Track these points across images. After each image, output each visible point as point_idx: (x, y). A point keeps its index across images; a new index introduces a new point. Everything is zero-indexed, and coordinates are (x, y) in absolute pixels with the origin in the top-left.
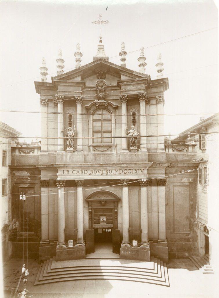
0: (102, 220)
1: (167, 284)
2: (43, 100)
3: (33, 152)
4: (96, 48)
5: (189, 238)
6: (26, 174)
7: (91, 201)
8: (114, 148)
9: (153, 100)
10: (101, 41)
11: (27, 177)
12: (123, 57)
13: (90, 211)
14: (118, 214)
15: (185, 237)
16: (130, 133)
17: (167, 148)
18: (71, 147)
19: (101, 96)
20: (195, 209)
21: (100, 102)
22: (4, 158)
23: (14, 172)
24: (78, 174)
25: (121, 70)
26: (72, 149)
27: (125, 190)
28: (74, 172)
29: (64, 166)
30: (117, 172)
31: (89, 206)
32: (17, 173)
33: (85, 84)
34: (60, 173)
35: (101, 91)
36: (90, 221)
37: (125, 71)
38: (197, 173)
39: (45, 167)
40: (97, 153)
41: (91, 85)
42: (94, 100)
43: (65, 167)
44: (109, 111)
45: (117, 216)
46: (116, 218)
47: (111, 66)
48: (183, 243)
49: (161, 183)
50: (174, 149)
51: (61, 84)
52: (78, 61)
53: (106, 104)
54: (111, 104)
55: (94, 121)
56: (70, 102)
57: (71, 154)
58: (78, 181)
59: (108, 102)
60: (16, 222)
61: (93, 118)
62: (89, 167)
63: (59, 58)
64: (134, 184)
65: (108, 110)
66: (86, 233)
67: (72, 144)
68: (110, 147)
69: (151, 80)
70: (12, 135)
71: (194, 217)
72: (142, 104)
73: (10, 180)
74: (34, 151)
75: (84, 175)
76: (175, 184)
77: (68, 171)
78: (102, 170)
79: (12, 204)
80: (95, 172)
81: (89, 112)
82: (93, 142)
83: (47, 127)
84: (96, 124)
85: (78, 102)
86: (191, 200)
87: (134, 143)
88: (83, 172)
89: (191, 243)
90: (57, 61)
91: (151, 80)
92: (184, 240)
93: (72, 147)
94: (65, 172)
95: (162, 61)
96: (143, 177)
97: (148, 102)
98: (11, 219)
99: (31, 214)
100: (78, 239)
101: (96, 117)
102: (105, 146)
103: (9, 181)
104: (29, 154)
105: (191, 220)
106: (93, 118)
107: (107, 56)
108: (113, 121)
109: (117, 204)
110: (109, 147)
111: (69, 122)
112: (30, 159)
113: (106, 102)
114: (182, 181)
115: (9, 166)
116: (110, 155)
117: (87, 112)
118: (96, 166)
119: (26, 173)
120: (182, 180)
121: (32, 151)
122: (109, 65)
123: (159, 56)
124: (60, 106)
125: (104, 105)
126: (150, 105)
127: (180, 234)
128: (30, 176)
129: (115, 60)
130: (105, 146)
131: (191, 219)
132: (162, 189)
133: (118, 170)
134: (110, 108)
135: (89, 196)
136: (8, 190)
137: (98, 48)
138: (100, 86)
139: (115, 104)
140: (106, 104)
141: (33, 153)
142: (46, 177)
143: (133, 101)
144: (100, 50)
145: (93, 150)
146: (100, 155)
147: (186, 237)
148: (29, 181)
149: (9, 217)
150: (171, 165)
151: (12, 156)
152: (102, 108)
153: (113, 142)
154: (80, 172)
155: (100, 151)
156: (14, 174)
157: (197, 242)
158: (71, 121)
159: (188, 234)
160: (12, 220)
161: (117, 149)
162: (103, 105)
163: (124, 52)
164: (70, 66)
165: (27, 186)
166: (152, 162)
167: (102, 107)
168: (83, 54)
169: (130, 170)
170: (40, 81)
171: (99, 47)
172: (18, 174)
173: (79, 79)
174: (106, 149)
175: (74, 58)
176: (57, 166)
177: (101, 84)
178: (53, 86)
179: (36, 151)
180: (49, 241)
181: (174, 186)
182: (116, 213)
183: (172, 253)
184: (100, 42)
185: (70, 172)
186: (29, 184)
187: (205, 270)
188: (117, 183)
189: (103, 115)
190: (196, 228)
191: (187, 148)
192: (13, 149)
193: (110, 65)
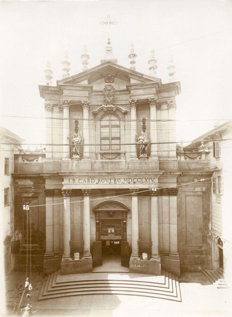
1: (178, 299)
3: (37, 159)
5: (202, 251)
6: (29, 183)
7: (99, 212)
8: (122, 155)
9: (165, 105)
10: (109, 43)
11: (30, 186)
12: (132, 59)
13: (98, 222)
15: (198, 250)
16: (139, 140)
17: (179, 155)
18: (77, 154)
19: (109, 101)
22: (6, 166)
23: (17, 181)
24: (85, 183)
25: (130, 73)
26: (78, 157)
27: (135, 199)
28: (80, 181)
29: (70, 174)
32: (20, 182)
34: (66, 181)
36: (98, 233)
38: (210, 182)
40: (104, 160)
42: (102, 105)
43: (71, 175)
45: (126, 227)
47: (120, 69)
49: (172, 192)
50: (186, 157)
51: (67, 88)
52: (85, 63)
53: (114, 109)
55: (102, 127)
57: (77, 161)
58: (85, 190)
60: (19, 234)
64: (144, 194)
65: (117, 116)
67: (78, 151)
68: (119, 154)
73: (13, 189)
74: (38, 158)
76: (187, 193)
77: (74, 180)
80: (103, 181)
82: (101, 150)
84: (103, 130)
88: (90, 180)
89: (204, 256)
93: (78, 155)
94: (71, 181)
98: (14, 230)
99: (35, 225)
100: (84, 251)
101: (104, 123)
103: (11, 191)
104: (33, 162)
105: (204, 232)
111: (76, 128)
112: (34, 167)
113: (114, 108)
114: (195, 191)
116: (118, 163)
118: (104, 174)
119: (30, 181)
124: (66, 111)
125: (112, 110)
126: (161, 110)
129: (124, 63)
130: (114, 154)
134: (118, 113)
136: (10, 200)
137: (106, 50)
139: (124, 109)
141: (37, 160)
143: (143, 106)
146: (108, 162)
147: (200, 250)
148: (33, 190)
149: (11, 228)
150: (183, 174)
151: (15, 164)
154: (87, 180)
155: (108, 158)
156: (17, 183)
157: (210, 255)
159: (201, 246)
160: (15, 232)
162: (111, 110)
164: (76, 69)
166: (163, 170)
169: (140, 179)
172: (21, 183)
173: (85, 83)
174: (114, 157)
176: (63, 174)
177: (109, 88)
179: (40, 158)
180: (53, 254)
181: (186, 196)
185: (77, 181)
186: (33, 194)
187: (219, 284)
190: (210, 240)
191: (200, 155)
192: (16, 157)
193: (119, 68)
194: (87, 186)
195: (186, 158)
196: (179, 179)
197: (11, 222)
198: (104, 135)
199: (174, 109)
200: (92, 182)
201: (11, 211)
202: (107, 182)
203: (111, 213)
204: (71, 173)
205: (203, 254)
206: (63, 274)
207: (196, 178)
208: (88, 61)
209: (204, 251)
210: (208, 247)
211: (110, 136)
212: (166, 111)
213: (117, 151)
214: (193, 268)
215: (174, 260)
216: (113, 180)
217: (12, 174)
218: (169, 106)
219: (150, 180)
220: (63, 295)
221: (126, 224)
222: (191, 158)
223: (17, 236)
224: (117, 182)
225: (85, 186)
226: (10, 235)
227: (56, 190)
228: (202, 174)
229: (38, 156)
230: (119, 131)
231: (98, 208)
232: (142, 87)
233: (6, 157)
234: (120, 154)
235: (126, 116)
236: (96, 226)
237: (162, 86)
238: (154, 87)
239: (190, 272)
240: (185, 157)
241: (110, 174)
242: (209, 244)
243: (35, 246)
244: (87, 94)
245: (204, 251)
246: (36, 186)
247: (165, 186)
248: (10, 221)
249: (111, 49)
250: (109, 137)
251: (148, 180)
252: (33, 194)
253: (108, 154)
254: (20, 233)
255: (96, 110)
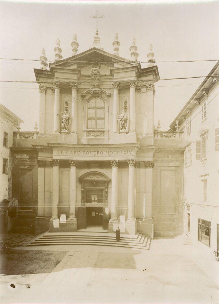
0: (94, 200)
3: (32, 136)
6: (26, 156)
7: (85, 182)
8: (106, 133)
10: (97, 34)
11: (26, 160)
13: (83, 190)
14: (109, 193)
18: (66, 129)
21: (95, 90)
22: (5, 140)
23: (14, 155)
25: (113, 59)
26: (66, 131)
27: (115, 169)
28: (68, 153)
29: (58, 145)
30: (108, 154)
31: (81, 186)
32: (17, 156)
33: (79, 71)
34: (55, 152)
36: (83, 200)
37: (117, 59)
40: (91, 137)
41: (87, 74)
43: (59, 146)
44: (102, 99)
45: (108, 195)
46: (106, 198)
47: (104, 55)
49: (150, 165)
51: (58, 71)
53: (100, 92)
54: (105, 92)
56: (65, 89)
57: (65, 135)
58: (71, 161)
60: (16, 201)
61: (123, 233)
62: (82, 148)
63: (56, 47)
64: (122, 165)
67: (67, 127)
68: (103, 132)
69: (142, 68)
72: (132, 90)
73: (11, 162)
74: (33, 135)
76: (163, 168)
77: (62, 152)
78: (94, 152)
79: (13, 184)
80: (88, 153)
81: (84, 100)
82: (87, 128)
85: (73, 88)
87: (123, 125)
88: (77, 152)
89: (176, 223)
90: (55, 51)
91: (142, 68)
94: (60, 152)
97: (138, 89)
98: (11, 197)
99: (29, 193)
103: (10, 162)
104: (29, 139)
106: (123, 233)
108: (106, 109)
109: (108, 184)
110: (102, 132)
111: (65, 107)
112: (28, 144)
113: (100, 91)
114: (169, 166)
115: (10, 148)
116: (102, 139)
117: (83, 99)
118: (88, 147)
119: (26, 155)
122: (103, 54)
128: (29, 159)
129: (108, 49)
132: (149, 170)
133: (108, 152)
136: (8, 170)
137: (94, 40)
138: (94, 75)
141: (32, 137)
144: (96, 42)
146: (93, 139)
148: (28, 163)
151: (14, 140)
152: (96, 96)
153: (105, 128)
154: (73, 152)
156: (15, 157)
157: (181, 222)
158: (67, 108)
159: (173, 214)
160: (12, 198)
163: (117, 42)
164: (67, 54)
166: (141, 148)
167: (96, 95)
169: (120, 151)
170: (40, 68)
171: (95, 39)
172: (18, 156)
173: (75, 67)
174: (98, 134)
175: (71, 48)
176: (52, 145)
177: (95, 73)
178: (51, 74)
179: (35, 135)
180: (44, 217)
182: (107, 192)
184: (96, 35)
185: (65, 152)
186: (28, 166)
187: (185, 242)
188: (107, 165)
189: (97, 108)
191: (175, 135)
192: (15, 134)
193: (104, 54)
195: (162, 137)
197: (9, 189)
199: (151, 93)
201: (9, 180)
204: (59, 144)
206: (50, 232)
212: (145, 94)
213: (102, 129)
216: (97, 153)
217: (10, 148)
218: (147, 89)
221: (108, 193)
223: (14, 202)
225: (72, 157)
226: (8, 199)
227: (48, 162)
229: (33, 133)
231: (83, 178)
233: (6, 132)
236: (82, 194)
237: (142, 71)
238: (134, 70)
239: (162, 237)
241: (93, 147)
243: (29, 211)
246: (31, 159)
248: (8, 188)
252: (28, 166)
253: (94, 132)
254: (16, 200)
255: (84, 92)
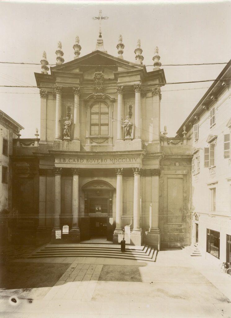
2: (43, 93)
3: (33, 143)
4: (96, 42)
5: (181, 229)
6: (26, 165)
9: (150, 93)
10: (100, 36)
12: (120, 49)
14: (113, 203)
15: (178, 228)
16: (125, 123)
17: (162, 141)
18: (68, 136)
20: (189, 200)
21: (98, 95)
25: (117, 62)
26: (69, 138)
28: (71, 161)
35: (99, 84)
38: (190, 166)
39: (44, 155)
40: (94, 144)
42: (92, 93)
43: (62, 155)
45: (112, 205)
47: (108, 58)
48: (176, 234)
51: (59, 75)
52: (78, 53)
53: (104, 97)
55: (92, 114)
56: (67, 95)
57: (68, 142)
59: (106, 95)
64: (128, 174)
65: (105, 103)
66: (81, 220)
67: (69, 134)
68: (107, 139)
70: (13, 127)
71: (186, 209)
74: (34, 143)
75: (80, 164)
76: (169, 176)
82: (90, 135)
83: (46, 119)
85: (76, 93)
86: (185, 192)
88: (80, 160)
89: (183, 234)
92: (177, 230)
93: (69, 136)
94: (62, 160)
95: (159, 54)
96: (136, 164)
102: (102, 138)
103: (9, 171)
104: (30, 146)
105: (184, 212)
107: (106, 50)
110: (105, 139)
111: (66, 113)
113: (103, 95)
114: (176, 174)
118: (92, 154)
120: (176, 172)
121: (32, 143)
123: (156, 49)
125: (102, 98)
127: (173, 225)
129: (113, 52)
130: (102, 138)
131: (184, 210)
132: (156, 179)
135: (85, 184)
137: (97, 43)
138: (98, 79)
139: (112, 97)
140: (104, 97)
142: (44, 166)
144: (100, 45)
145: (90, 142)
147: (179, 228)
148: (29, 171)
149: (9, 204)
150: (167, 159)
157: (189, 233)
161: (113, 141)
165: (27, 177)
166: (147, 155)
168: (81, 46)
169: (125, 159)
174: (102, 141)
177: (98, 76)
179: (36, 142)
181: (168, 178)
183: (165, 243)
186: (29, 175)
189: (101, 114)
190: (189, 219)
191: (182, 141)
193: (108, 57)
194: (76, 165)
196: (162, 163)
198: (94, 122)
200: (81, 162)
202: (95, 162)
203: (98, 192)
205: (182, 232)
206: (52, 244)
207: (177, 162)
208: (80, 51)
209: (183, 229)
210: (187, 225)
211: (100, 123)
212: (151, 98)
214: (172, 245)
215: (155, 235)
219: (134, 160)
220: (48, 256)
222: (173, 143)
223: (15, 213)
224: (104, 161)
228: (183, 157)
230: (108, 118)
232: (128, 75)
234: (108, 138)
235: (114, 104)
236: (85, 204)
240: (167, 142)
241: (97, 154)
242: (188, 222)
244: (78, 81)
245: (183, 229)
247: (148, 168)
249: (102, 42)
250: (98, 123)
251: (131, 160)
